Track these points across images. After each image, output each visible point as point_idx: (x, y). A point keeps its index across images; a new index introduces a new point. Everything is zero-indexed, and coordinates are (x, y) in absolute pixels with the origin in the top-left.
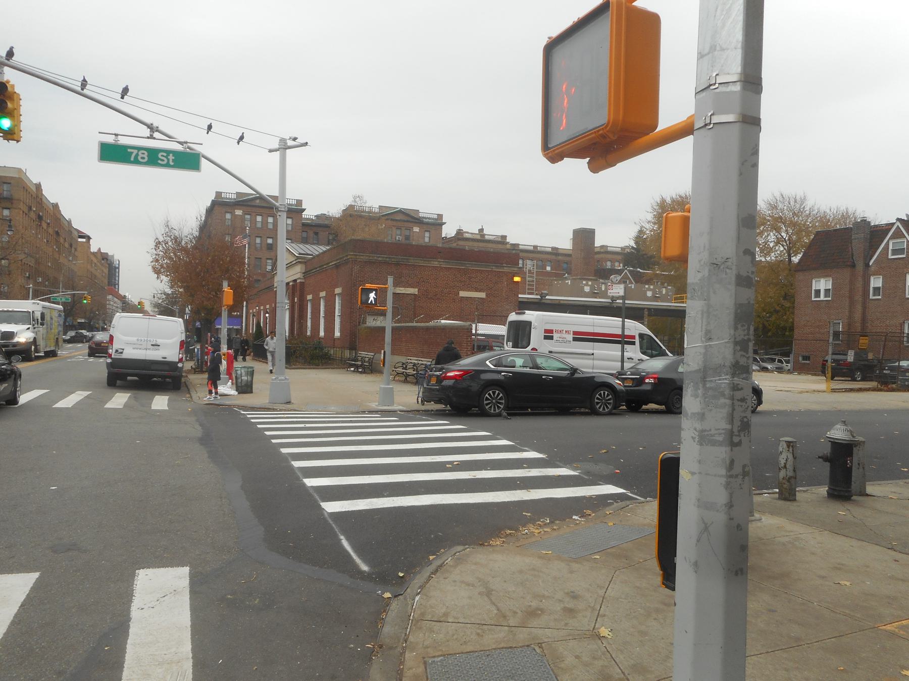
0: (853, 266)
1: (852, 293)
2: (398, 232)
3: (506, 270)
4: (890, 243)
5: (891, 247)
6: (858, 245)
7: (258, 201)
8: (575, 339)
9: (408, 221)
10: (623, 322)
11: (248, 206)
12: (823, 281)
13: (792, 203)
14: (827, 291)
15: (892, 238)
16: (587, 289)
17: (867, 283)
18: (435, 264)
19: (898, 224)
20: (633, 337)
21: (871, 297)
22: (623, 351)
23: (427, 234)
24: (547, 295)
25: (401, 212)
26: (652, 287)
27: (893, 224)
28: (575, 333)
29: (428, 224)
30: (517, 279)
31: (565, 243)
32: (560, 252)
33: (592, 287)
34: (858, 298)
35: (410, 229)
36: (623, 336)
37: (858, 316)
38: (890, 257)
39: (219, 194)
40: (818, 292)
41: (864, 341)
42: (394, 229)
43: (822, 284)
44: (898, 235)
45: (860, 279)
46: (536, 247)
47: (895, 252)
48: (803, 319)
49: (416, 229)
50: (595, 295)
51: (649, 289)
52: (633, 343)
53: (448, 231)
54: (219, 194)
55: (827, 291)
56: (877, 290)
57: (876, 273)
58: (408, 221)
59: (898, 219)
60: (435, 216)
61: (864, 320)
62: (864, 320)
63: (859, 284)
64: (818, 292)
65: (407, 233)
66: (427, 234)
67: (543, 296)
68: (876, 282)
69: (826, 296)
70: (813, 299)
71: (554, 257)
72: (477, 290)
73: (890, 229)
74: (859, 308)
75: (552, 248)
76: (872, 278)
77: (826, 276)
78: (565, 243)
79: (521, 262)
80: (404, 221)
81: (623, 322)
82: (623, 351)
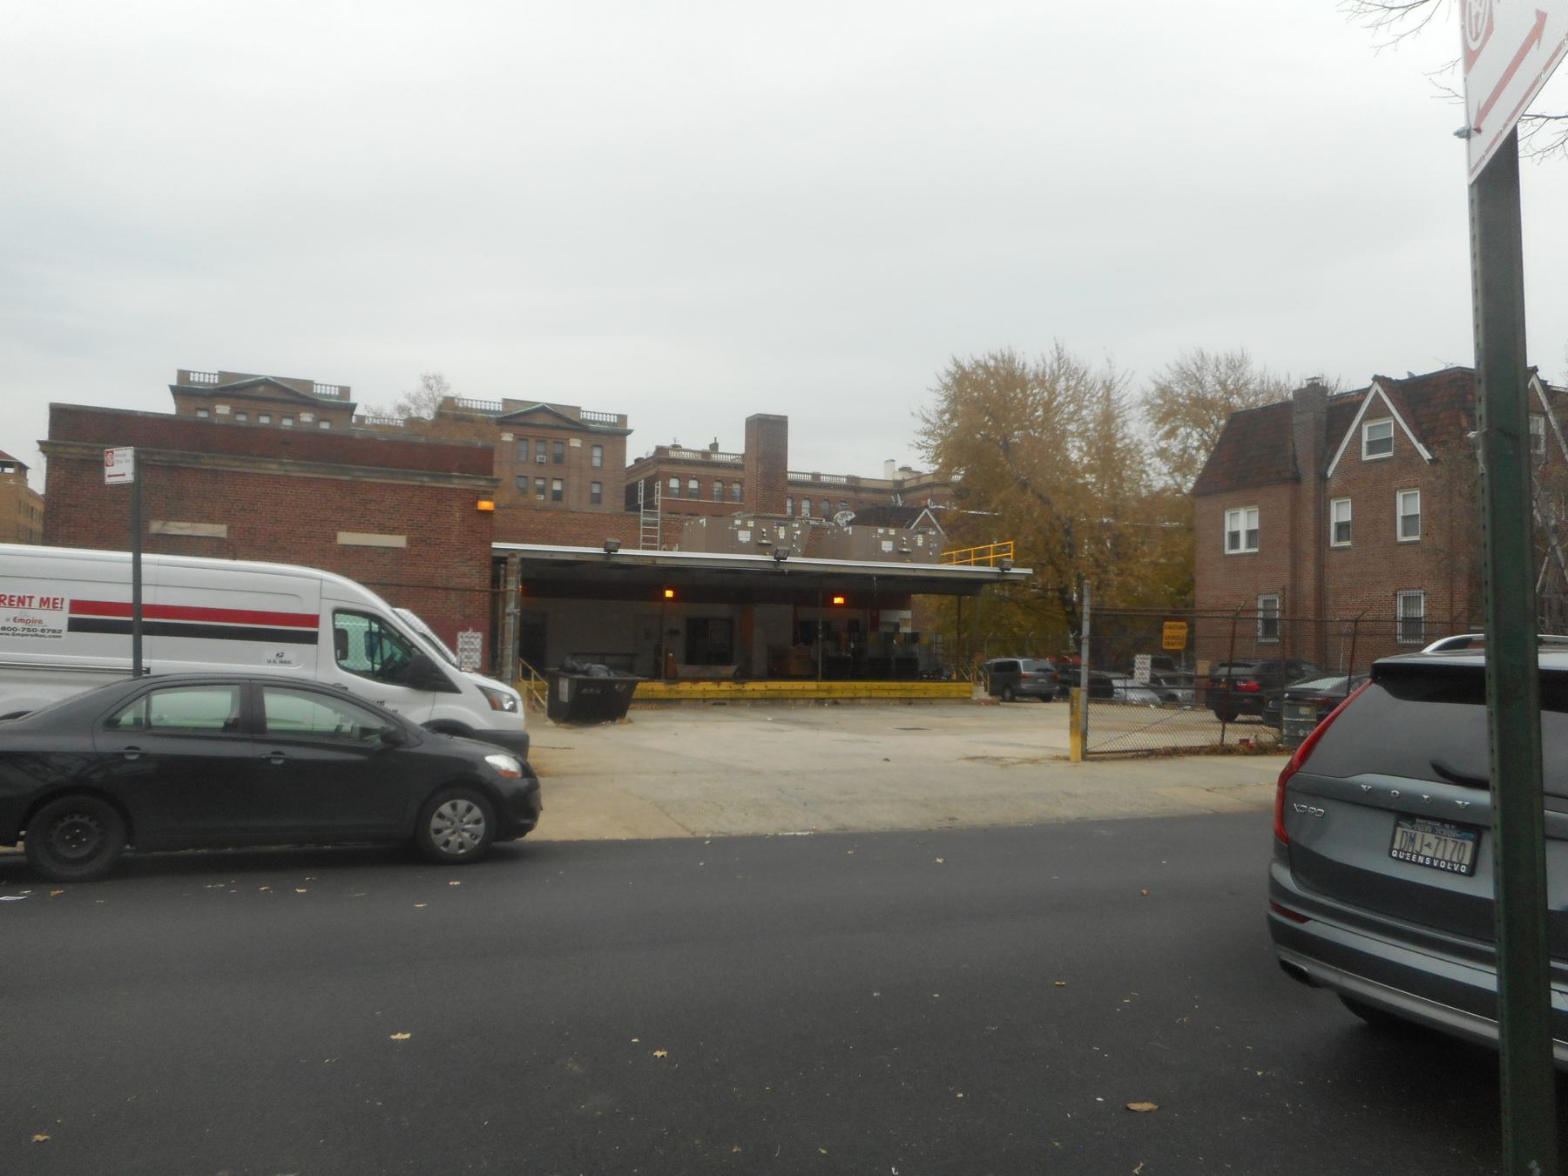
0: (1296, 480)
1: (1298, 535)
2: (541, 448)
3: (456, 484)
4: (1363, 430)
5: (1365, 438)
6: (1303, 442)
7: (261, 389)
8: (75, 626)
9: (558, 428)
10: (137, 564)
11: (238, 397)
12: (1243, 513)
13: (1222, 368)
14: (1251, 533)
15: (1369, 416)
16: (744, 536)
17: (1323, 516)
18: (272, 468)
19: (1377, 387)
20: (313, 620)
21: (1333, 543)
22: (137, 654)
23: (597, 453)
24: (619, 546)
25: (544, 410)
26: (892, 532)
27: (1368, 389)
28: (76, 606)
29: (598, 433)
30: (485, 505)
31: (734, 445)
32: (863, 484)
33: (755, 532)
34: (1308, 547)
35: (563, 442)
36: (137, 608)
37: (1308, 584)
38: (1365, 457)
39: (183, 375)
40: (1235, 536)
41: (1174, 633)
42: (532, 441)
43: (1242, 521)
44: (1377, 410)
45: (1310, 507)
46: (816, 476)
47: (1374, 447)
48: (1211, 591)
49: (575, 443)
50: (899, 555)
51: (886, 537)
52: (312, 639)
53: (638, 448)
54: (183, 375)
55: (1251, 533)
56: (1342, 527)
57: (1340, 494)
58: (558, 428)
59: (1377, 379)
60: (613, 419)
61: (1320, 594)
62: (1320, 594)
63: (1308, 518)
64: (1235, 536)
65: (558, 449)
66: (597, 453)
67: (610, 550)
68: (1341, 512)
69: (1249, 545)
70: (1228, 551)
71: (851, 494)
72: (383, 530)
73: (1360, 403)
74: (1309, 567)
75: (849, 478)
76: (1333, 504)
77: (1246, 504)
78: (734, 445)
79: (789, 504)
80: (553, 428)
81: (137, 564)
82: (137, 654)
